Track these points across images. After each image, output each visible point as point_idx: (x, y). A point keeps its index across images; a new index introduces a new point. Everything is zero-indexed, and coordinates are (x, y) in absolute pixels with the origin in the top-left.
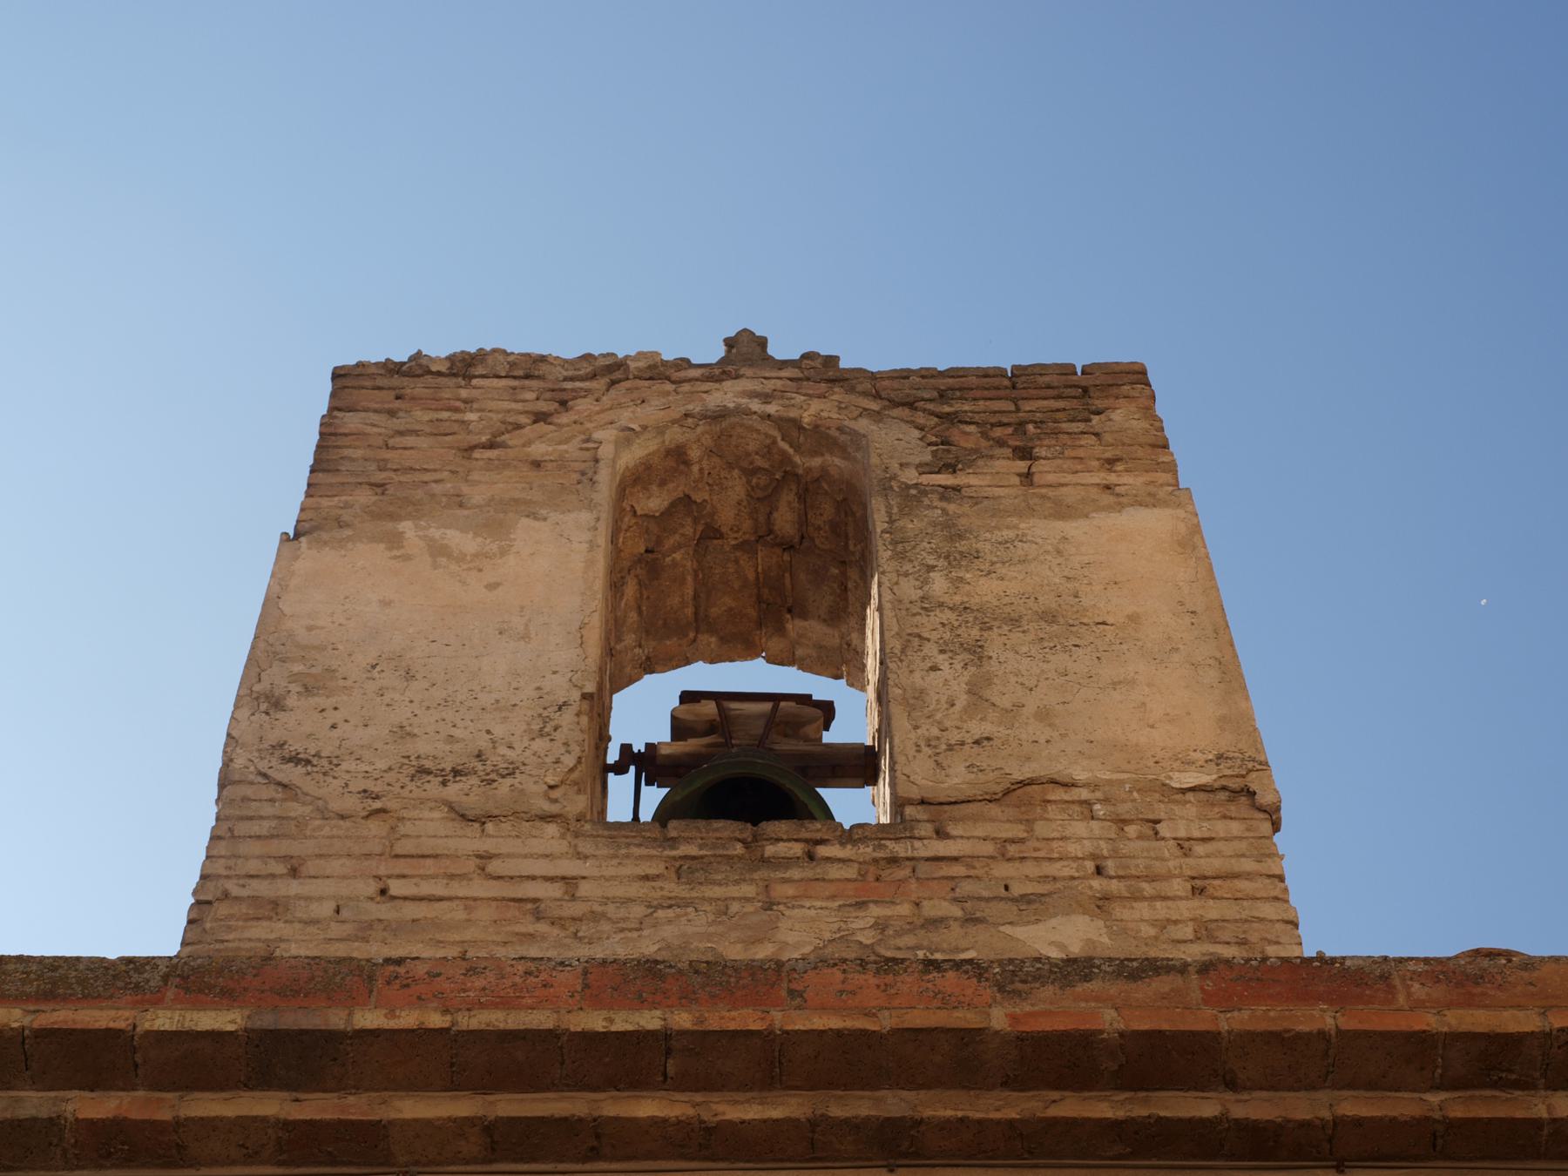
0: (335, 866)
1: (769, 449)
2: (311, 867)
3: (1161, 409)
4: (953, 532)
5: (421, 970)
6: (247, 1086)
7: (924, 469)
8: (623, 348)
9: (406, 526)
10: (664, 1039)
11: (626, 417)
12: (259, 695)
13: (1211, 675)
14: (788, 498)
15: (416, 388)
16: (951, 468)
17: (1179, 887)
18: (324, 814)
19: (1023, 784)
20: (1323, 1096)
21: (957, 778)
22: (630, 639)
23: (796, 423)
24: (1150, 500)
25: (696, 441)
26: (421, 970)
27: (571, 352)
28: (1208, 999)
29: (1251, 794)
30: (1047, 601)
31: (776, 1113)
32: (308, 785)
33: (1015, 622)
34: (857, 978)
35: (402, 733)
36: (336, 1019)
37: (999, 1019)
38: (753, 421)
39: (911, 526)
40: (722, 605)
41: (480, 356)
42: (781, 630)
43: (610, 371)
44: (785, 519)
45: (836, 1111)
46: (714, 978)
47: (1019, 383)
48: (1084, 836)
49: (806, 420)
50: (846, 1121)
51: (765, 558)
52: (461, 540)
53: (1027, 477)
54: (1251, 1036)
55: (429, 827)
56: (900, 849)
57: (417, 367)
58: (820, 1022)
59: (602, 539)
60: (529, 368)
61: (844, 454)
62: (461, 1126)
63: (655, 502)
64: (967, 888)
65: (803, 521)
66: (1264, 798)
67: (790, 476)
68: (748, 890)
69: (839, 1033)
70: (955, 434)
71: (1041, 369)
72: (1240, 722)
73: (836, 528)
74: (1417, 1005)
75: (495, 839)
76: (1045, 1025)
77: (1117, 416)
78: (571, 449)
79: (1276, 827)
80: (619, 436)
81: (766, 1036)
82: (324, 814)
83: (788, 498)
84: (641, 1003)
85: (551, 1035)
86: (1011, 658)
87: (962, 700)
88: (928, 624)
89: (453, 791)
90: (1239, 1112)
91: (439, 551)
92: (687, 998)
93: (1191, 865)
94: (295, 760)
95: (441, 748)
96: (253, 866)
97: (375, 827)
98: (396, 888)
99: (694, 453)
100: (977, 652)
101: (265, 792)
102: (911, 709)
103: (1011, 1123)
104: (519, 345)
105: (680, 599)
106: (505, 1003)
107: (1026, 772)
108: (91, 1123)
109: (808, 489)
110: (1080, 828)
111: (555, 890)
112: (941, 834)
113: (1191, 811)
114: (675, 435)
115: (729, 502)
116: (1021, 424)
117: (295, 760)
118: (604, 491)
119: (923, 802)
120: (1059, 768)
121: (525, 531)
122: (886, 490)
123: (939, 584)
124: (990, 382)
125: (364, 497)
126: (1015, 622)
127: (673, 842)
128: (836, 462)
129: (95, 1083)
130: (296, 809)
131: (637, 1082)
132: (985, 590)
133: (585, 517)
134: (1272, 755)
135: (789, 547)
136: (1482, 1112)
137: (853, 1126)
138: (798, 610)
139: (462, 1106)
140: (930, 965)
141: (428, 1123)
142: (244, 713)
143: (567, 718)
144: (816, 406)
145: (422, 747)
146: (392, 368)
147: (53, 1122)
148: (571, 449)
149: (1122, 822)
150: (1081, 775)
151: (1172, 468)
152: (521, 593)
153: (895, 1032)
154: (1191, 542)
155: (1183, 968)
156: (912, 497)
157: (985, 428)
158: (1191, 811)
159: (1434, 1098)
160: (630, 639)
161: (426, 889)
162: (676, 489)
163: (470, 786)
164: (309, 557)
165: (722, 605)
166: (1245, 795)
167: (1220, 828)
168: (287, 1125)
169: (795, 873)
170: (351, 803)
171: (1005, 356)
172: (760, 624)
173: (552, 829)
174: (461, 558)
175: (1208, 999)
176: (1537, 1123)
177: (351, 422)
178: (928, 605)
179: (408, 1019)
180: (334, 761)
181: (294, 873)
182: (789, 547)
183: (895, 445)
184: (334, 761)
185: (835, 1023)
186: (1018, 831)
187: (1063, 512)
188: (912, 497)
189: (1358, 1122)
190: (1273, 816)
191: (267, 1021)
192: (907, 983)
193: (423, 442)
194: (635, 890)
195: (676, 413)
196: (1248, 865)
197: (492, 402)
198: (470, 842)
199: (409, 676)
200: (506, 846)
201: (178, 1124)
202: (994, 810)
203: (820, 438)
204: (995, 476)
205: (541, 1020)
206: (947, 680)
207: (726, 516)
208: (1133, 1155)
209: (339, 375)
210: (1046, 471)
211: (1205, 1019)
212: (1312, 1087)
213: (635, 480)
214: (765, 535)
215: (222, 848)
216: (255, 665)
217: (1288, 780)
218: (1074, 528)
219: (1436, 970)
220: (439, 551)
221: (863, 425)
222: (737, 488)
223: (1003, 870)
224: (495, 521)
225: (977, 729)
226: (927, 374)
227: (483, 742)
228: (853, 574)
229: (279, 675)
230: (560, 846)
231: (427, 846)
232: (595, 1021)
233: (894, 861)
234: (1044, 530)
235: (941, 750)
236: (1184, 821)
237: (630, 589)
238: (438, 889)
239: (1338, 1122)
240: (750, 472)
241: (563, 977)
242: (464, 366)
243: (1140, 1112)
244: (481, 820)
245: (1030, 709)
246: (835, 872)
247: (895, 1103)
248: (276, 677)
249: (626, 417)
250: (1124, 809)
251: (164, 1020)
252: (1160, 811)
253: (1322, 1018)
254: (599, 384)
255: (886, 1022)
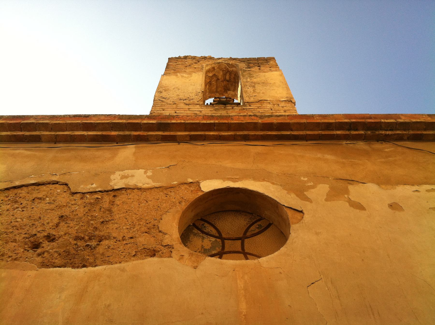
0: (169, 109)
1: (226, 67)
2: (166, 110)
3: (277, 62)
4: (250, 74)
5: (181, 116)
6: (157, 131)
7: (246, 68)
8: (206, 55)
9: (178, 74)
10: (214, 124)
11: (207, 63)
12: (159, 91)
13: (285, 89)
14: (228, 74)
15: (180, 60)
16: (250, 68)
17: (282, 111)
18: (167, 104)
19: (261, 100)
20: (305, 132)
21: (252, 100)
22: (207, 93)
23: (229, 64)
24: (276, 71)
25: (216, 66)
26: (181, 116)
27: (200, 56)
28: (288, 119)
29: (291, 101)
30: (263, 81)
31: (230, 134)
32: (165, 101)
33: (259, 83)
34: (241, 117)
35: (178, 95)
36: (169, 122)
37: (260, 121)
38: (223, 64)
39: (244, 74)
40: (219, 89)
41: (188, 56)
42: (227, 93)
43: (205, 58)
44: (227, 77)
45: (238, 134)
46: (221, 117)
47: (258, 59)
48: (269, 106)
49: (230, 63)
50: (239, 135)
51: (225, 83)
52: (186, 76)
53: (260, 69)
54: (295, 123)
55: (182, 105)
56: (245, 108)
57: (179, 58)
58: (235, 122)
59: (204, 75)
60: (194, 58)
61: (236, 68)
62: (186, 136)
63: (211, 75)
64: (254, 112)
65: (230, 77)
66: (293, 101)
67: (228, 71)
68: (224, 112)
69: (238, 123)
70: (250, 64)
71: (261, 58)
72: (290, 94)
73: (234, 78)
74: (317, 119)
75: (190, 107)
76: (266, 122)
77: (271, 62)
78: (200, 66)
79: (295, 105)
80: (206, 66)
81: (228, 123)
82: (167, 104)
83: (228, 74)
84: (211, 120)
85: (199, 123)
86: (259, 88)
87: (252, 92)
88: (247, 84)
89: (185, 101)
90: (293, 133)
91: (182, 76)
92: (217, 119)
93: (284, 109)
94: (164, 98)
95: (183, 97)
96: (158, 109)
97: (174, 106)
98: (177, 112)
99: (216, 68)
100: (254, 87)
101: (159, 101)
102: (245, 92)
103: (262, 135)
104: (192, 55)
105: (214, 88)
106: (192, 120)
107: (261, 99)
108: (135, 135)
109: (231, 73)
110: (269, 105)
111: (199, 112)
112: (250, 106)
113: (283, 103)
114: (213, 65)
115: (220, 75)
116: (258, 64)
117: (164, 98)
118: (204, 71)
119: (248, 103)
120: (266, 99)
121: (194, 74)
122: (241, 70)
123: (249, 80)
124: (254, 59)
125: (173, 71)
126: (259, 83)
127: (214, 107)
128: (234, 69)
129: (136, 130)
130: (164, 103)
131: (210, 130)
132: (255, 80)
133: (202, 73)
134: (294, 97)
135: (228, 81)
136: (327, 133)
137: (240, 136)
138: (229, 90)
139: (187, 133)
140: (250, 115)
141: (182, 135)
142: (157, 93)
143: (200, 94)
144: (231, 62)
145: (180, 97)
146: (176, 58)
147: (130, 135)
148: (200, 66)
149: (274, 105)
150: (268, 99)
151: (279, 68)
152: (194, 83)
153: (246, 123)
154: (282, 75)
155: (285, 116)
156: (245, 71)
157: (254, 64)
158: (283, 103)
159: (320, 132)
160: (207, 93)
161: (181, 112)
162: (213, 73)
163: (188, 102)
164: (165, 77)
165: (219, 89)
166: (290, 101)
167: (287, 105)
168: (162, 136)
169: (231, 110)
170: (171, 103)
171: (256, 57)
172: (224, 92)
173: (198, 106)
174: (186, 77)
175: (288, 119)
176: (334, 135)
177: (171, 63)
178: (247, 82)
179: (179, 121)
180: (169, 98)
181: (163, 110)
182: (228, 81)
183: (242, 65)
184: (169, 98)
185: (237, 122)
186: (260, 106)
187: (265, 72)
188: (245, 71)
189: (309, 135)
190: (294, 103)
191: (159, 122)
192: (247, 117)
193: (180, 66)
194: (209, 112)
195: (213, 62)
196: (292, 109)
197: (189, 61)
198: (187, 107)
199: (179, 89)
200: (192, 107)
201: (147, 135)
202: (257, 103)
203: (232, 66)
204: (256, 69)
205: (198, 121)
206: (251, 90)
207: (220, 77)
208: (278, 139)
209: (169, 59)
210: (262, 68)
211: (288, 121)
212: (303, 131)
213: (208, 71)
214: (225, 80)
215: (154, 108)
216: (158, 88)
217: (296, 99)
218: (266, 74)
219: (320, 116)
220: (182, 76)
221: (238, 63)
222: (221, 73)
223: (258, 110)
224: (190, 73)
225: (254, 95)
226: (246, 58)
227: (189, 96)
228: (236, 84)
229: (161, 89)
230: (199, 107)
231: (182, 107)
232: (205, 122)
233: (244, 109)
234: (262, 74)
235: (249, 97)
236: (283, 104)
237: (208, 86)
238: (183, 112)
239: (307, 135)
240: (223, 71)
241: (200, 117)
242: (185, 57)
243: (279, 133)
244: (189, 105)
245: (261, 92)
246: (236, 110)
247: (246, 133)
248: (161, 89)
249: (207, 63)
250: (274, 103)
251: (145, 122)
252: (279, 103)
253: (304, 121)
254: (203, 60)
255: (245, 122)
